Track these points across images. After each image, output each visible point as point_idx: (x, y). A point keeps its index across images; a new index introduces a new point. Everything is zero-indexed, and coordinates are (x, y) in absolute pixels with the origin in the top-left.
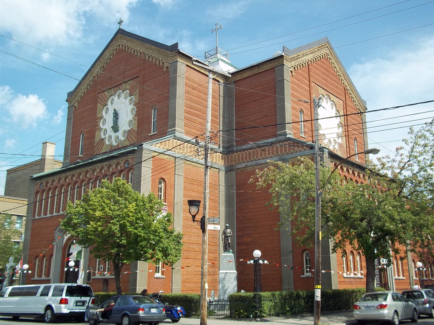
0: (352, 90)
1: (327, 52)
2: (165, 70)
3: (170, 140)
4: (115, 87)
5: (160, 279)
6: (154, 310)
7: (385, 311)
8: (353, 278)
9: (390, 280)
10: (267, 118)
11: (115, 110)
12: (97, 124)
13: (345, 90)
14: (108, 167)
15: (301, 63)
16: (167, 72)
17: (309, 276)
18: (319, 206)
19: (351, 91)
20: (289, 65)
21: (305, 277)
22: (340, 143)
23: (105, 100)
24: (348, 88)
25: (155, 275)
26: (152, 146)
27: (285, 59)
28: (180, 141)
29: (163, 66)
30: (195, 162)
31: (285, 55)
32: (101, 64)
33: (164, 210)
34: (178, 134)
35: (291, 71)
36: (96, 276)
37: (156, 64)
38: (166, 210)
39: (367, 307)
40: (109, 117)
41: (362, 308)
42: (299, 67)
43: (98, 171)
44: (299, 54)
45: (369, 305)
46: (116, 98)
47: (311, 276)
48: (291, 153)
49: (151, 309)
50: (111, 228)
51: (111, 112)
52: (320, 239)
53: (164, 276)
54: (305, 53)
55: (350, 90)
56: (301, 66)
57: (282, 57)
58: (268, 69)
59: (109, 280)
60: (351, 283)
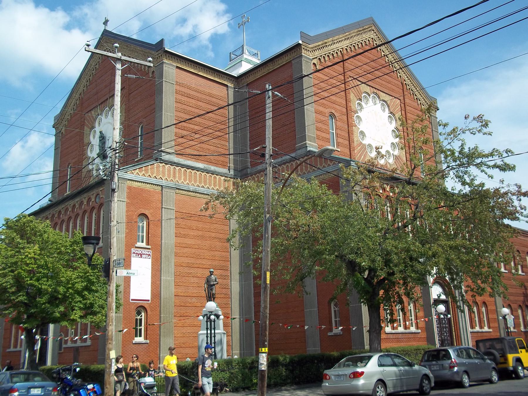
0: (413, 85)
1: (372, 36)
2: (151, 76)
3: (153, 164)
4: (102, 103)
5: (142, 345)
6: (435, 367)
7: (361, 382)
8: (401, 333)
9: (464, 334)
10: (285, 128)
11: (101, 132)
12: (84, 152)
13: (403, 86)
14: (80, 204)
15: (330, 53)
16: (153, 77)
17: (337, 333)
18: (267, 236)
19: (413, 86)
20: (311, 56)
21: (333, 334)
22: (395, 156)
23: (91, 121)
24: (408, 82)
25: (134, 339)
26: (126, 173)
27: (304, 48)
28: (170, 165)
29: (148, 70)
30: (192, 192)
31: (304, 44)
32: (86, 77)
33: (147, 254)
34: (165, 157)
35: (314, 64)
36: (334, 332)
37: (141, 70)
38: (149, 255)
39: (339, 376)
40: (95, 141)
41: (333, 377)
42: (327, 58)
43: (70, 210)
44: (326, 41)
45: (340, 373)
46: (103, 118)
47: (340, 333)
48: (313, 171)
49: (32, 389)
50: (27, 283)
51: (98, 135)
52: (268, 282)
53: (148, 341)
54: (336, 40)
55: (411, 85)
56: (331, 57)
57: (298, 45)
58: (284, 63)
59: (80, 348)
60: (398, 340)
